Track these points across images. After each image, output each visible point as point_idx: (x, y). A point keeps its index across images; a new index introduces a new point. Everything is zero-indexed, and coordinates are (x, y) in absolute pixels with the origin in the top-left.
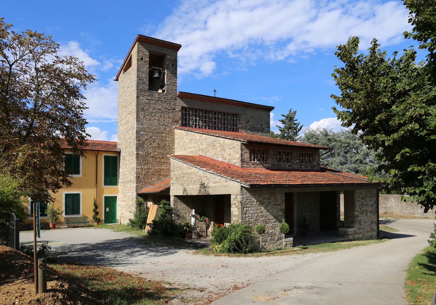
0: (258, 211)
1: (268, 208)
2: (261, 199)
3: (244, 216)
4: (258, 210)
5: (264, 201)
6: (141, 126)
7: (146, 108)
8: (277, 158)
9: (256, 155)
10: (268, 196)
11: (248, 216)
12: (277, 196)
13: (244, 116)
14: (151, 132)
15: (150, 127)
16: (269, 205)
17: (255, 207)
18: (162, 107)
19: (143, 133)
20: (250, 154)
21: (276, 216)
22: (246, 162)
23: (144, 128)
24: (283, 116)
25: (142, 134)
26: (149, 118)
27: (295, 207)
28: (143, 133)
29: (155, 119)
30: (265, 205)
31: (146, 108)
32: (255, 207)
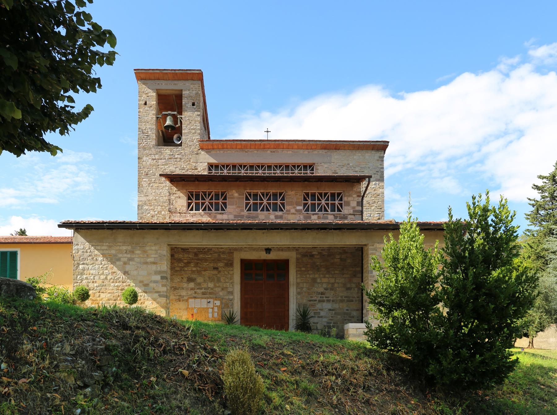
0: (107, 271)
1: (128, 268)
2: (113, 252)
3: (79, 276)
4: (106, 269)
5: (120, 255)
6: (144, 199)
7: (151, 172)
8: (247, 204)
9: (200, 201)
10: (129, 248)
11: (87, 278)
12: (147, 248)
13: (326, 166)
14: (159, 206)
15: (157, 198)
16: (131, 263)
17: (101, 264)
18: (176, 168)
19: (147, 207)
20: (189, 198)
21: (145, 282)
22: (179, 213)
23: (149, 201)
24: (541, 177)
25: (147, 210)
26: (156, 185)
27: (293, 291)
28: (147, 207)
29: (166, 186)
30: (121, 263)
31: (151, 172)
32: (101, 264)
